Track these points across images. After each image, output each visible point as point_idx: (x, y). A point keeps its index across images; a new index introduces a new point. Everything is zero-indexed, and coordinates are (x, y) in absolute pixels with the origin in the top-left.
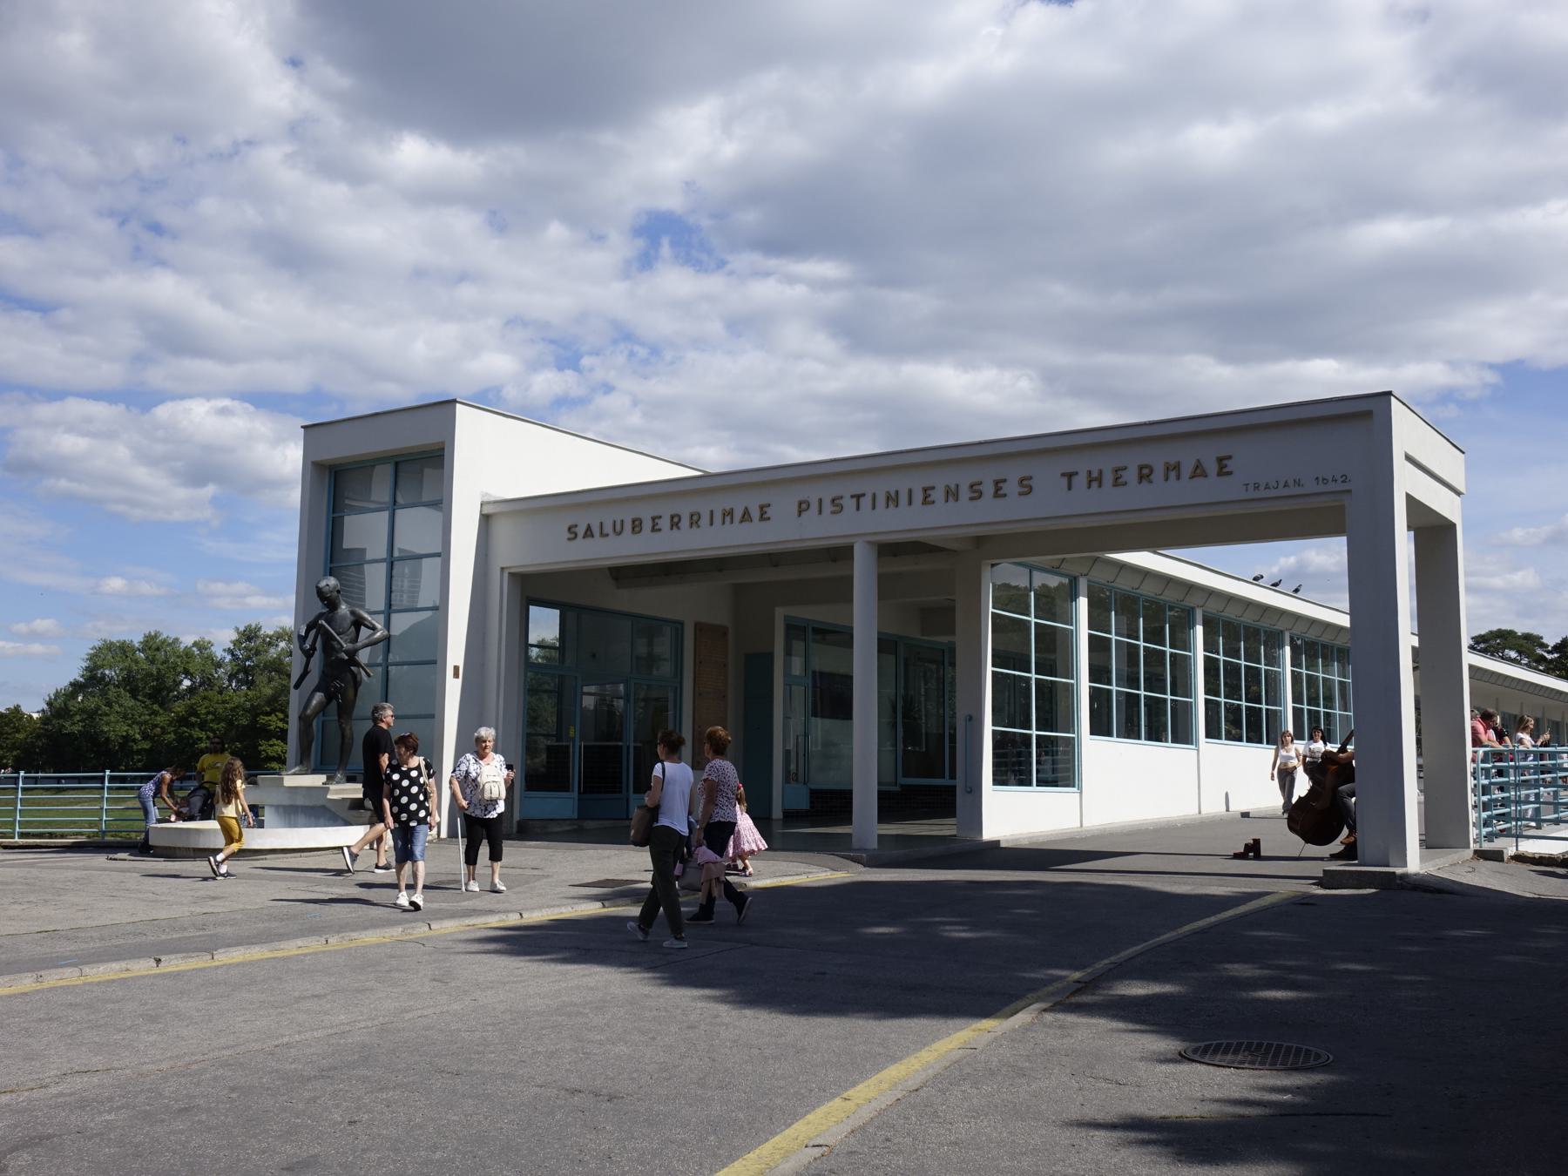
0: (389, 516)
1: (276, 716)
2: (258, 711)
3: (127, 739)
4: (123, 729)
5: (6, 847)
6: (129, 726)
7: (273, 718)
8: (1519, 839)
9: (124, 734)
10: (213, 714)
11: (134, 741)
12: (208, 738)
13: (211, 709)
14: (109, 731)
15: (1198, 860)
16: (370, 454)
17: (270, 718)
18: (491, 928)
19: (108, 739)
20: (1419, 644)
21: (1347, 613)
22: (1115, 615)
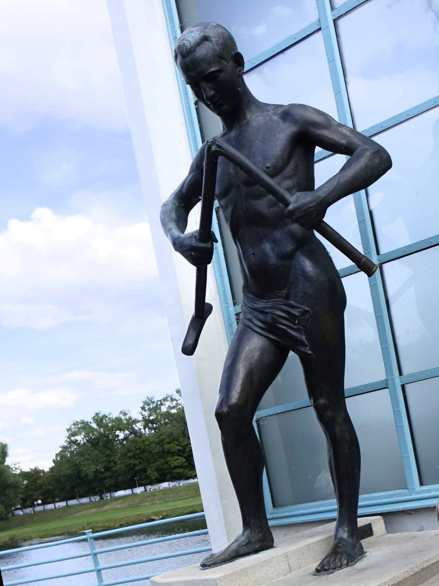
0: (373, 137)
1: (174, 443)
2: (164, 443)
3: (96, 472)
4: (93, 468)
5: (436, 497)
6: (96, 465)
7: (172, 445)
8: (95, 573)
9: (95, 470)
10: (139, 449)
11: (101, 472)
12: (140, 463)
13: (138, 447)
14: (87, 470)
15: (126, 568)
16: (175, 191)
17: (171, 445)
18: (157, 575)
19: (86, 475)
20: (289, 351)
21: (360, 271)
22: (373, 269)
